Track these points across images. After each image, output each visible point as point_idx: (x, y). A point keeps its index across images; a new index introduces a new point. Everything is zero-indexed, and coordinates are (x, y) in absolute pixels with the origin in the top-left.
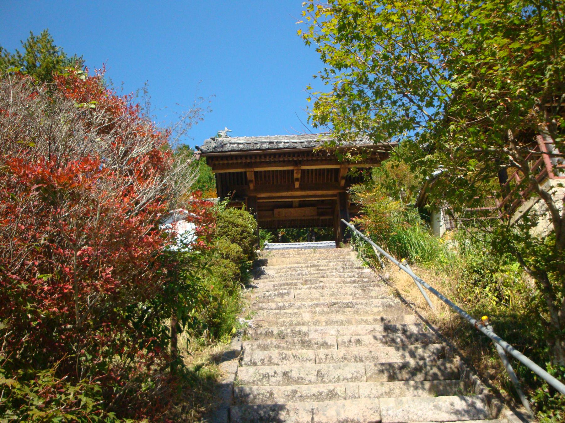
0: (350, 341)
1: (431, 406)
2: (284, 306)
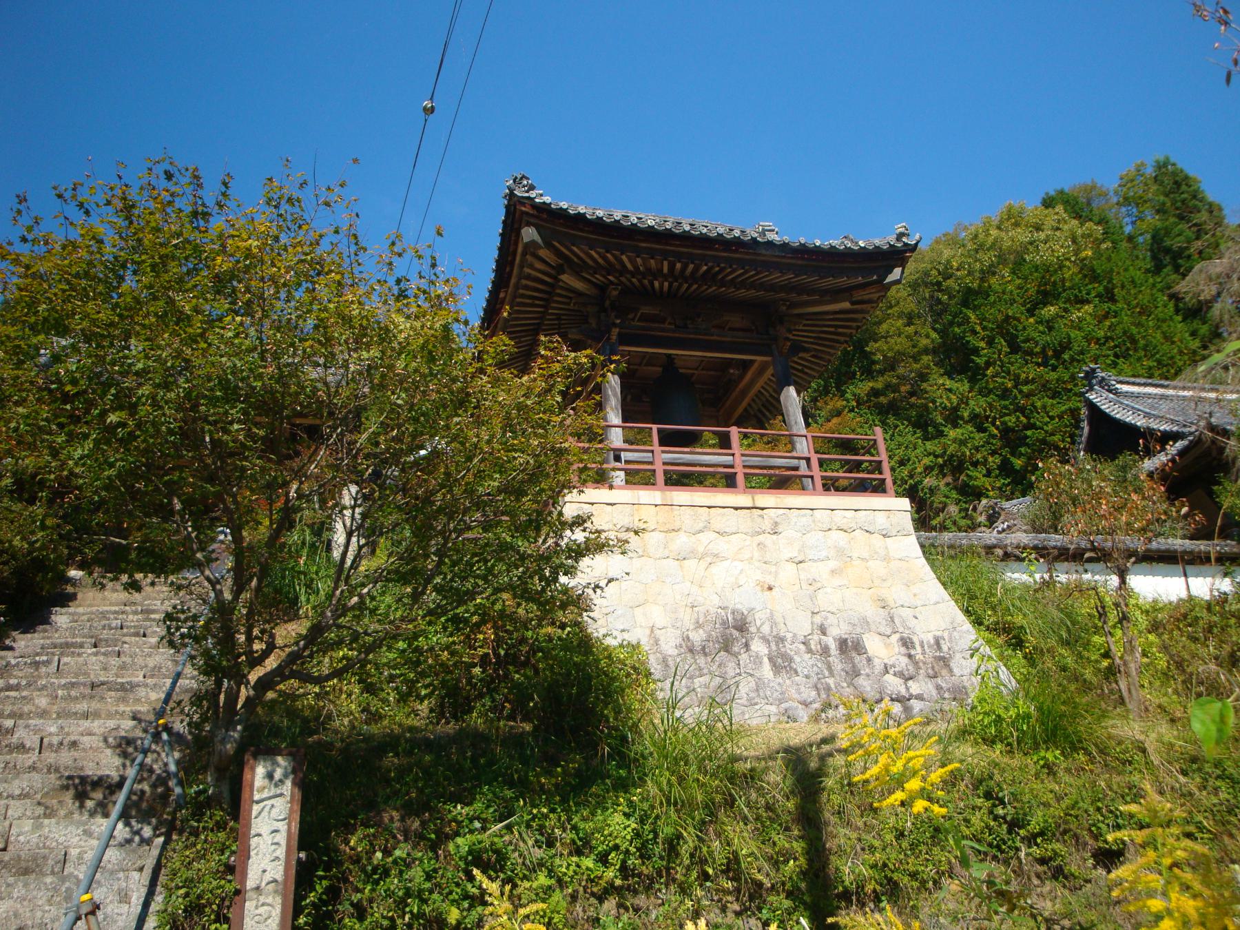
0: (61, 744)
1: (80, 831)
2: (19, 684)
